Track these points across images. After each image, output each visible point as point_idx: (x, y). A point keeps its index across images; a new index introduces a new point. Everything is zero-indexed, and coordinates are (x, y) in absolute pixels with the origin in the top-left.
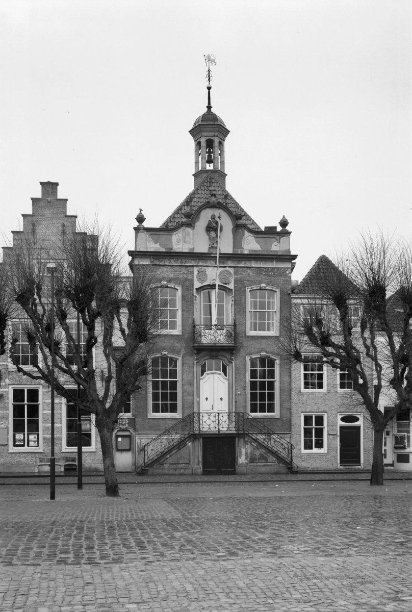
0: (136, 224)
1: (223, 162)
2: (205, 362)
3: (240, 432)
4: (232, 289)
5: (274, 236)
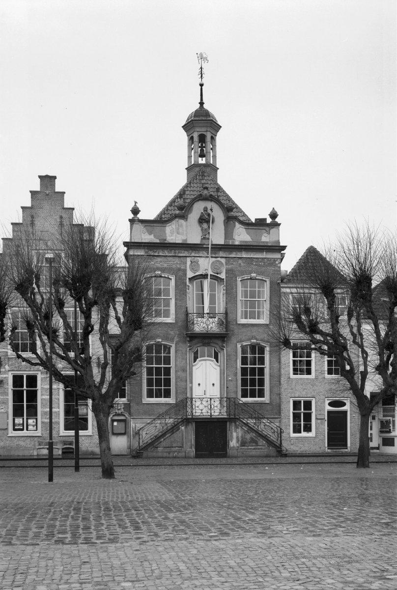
0: (131, 216)
1: (214, 157)
2: (198, 349)
3: (231, 417)
4: (223, 279)
5: (264, 228)
